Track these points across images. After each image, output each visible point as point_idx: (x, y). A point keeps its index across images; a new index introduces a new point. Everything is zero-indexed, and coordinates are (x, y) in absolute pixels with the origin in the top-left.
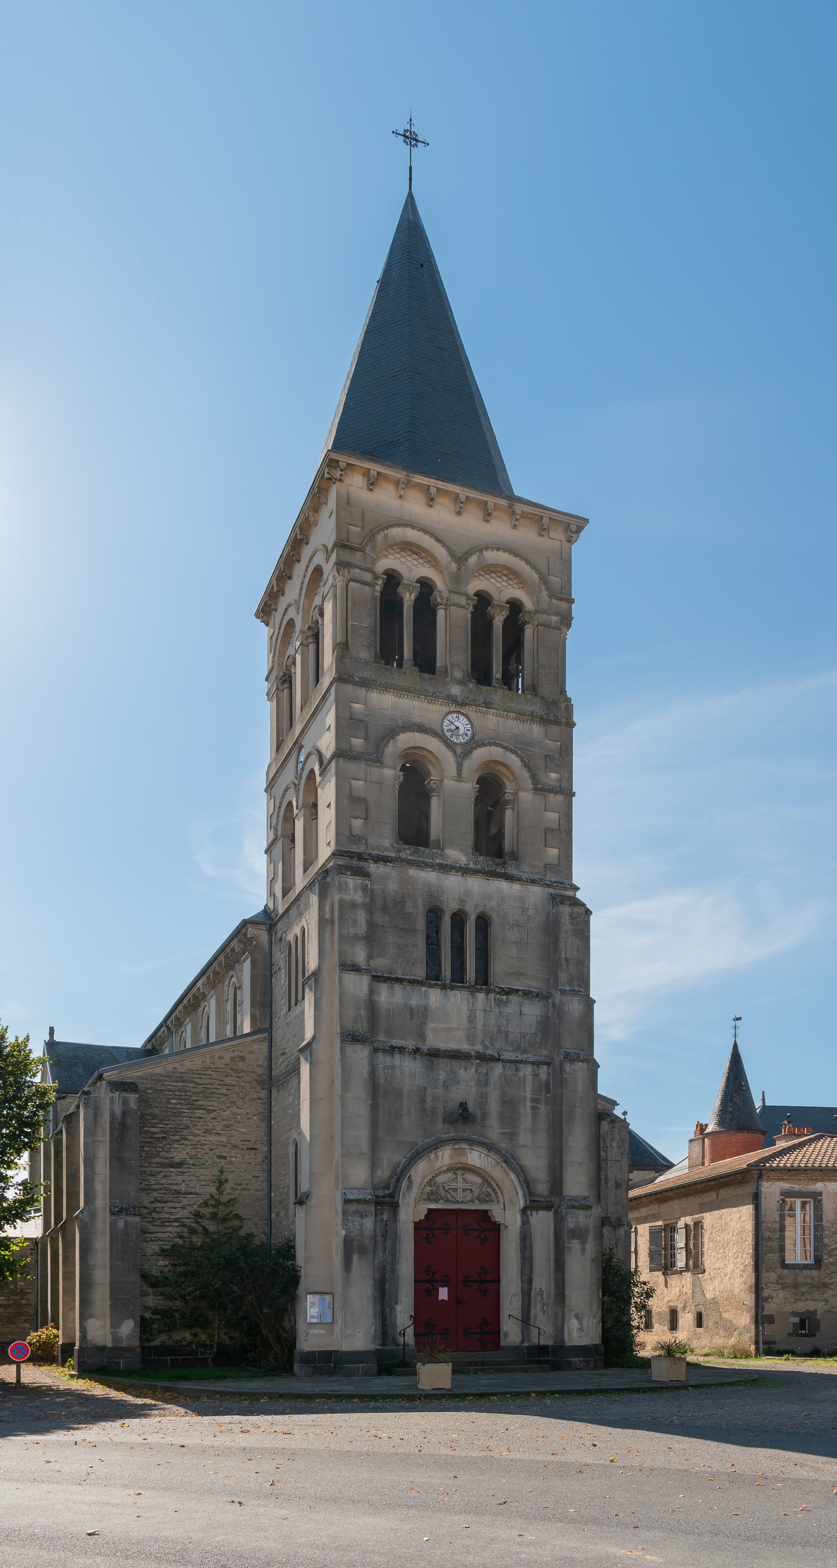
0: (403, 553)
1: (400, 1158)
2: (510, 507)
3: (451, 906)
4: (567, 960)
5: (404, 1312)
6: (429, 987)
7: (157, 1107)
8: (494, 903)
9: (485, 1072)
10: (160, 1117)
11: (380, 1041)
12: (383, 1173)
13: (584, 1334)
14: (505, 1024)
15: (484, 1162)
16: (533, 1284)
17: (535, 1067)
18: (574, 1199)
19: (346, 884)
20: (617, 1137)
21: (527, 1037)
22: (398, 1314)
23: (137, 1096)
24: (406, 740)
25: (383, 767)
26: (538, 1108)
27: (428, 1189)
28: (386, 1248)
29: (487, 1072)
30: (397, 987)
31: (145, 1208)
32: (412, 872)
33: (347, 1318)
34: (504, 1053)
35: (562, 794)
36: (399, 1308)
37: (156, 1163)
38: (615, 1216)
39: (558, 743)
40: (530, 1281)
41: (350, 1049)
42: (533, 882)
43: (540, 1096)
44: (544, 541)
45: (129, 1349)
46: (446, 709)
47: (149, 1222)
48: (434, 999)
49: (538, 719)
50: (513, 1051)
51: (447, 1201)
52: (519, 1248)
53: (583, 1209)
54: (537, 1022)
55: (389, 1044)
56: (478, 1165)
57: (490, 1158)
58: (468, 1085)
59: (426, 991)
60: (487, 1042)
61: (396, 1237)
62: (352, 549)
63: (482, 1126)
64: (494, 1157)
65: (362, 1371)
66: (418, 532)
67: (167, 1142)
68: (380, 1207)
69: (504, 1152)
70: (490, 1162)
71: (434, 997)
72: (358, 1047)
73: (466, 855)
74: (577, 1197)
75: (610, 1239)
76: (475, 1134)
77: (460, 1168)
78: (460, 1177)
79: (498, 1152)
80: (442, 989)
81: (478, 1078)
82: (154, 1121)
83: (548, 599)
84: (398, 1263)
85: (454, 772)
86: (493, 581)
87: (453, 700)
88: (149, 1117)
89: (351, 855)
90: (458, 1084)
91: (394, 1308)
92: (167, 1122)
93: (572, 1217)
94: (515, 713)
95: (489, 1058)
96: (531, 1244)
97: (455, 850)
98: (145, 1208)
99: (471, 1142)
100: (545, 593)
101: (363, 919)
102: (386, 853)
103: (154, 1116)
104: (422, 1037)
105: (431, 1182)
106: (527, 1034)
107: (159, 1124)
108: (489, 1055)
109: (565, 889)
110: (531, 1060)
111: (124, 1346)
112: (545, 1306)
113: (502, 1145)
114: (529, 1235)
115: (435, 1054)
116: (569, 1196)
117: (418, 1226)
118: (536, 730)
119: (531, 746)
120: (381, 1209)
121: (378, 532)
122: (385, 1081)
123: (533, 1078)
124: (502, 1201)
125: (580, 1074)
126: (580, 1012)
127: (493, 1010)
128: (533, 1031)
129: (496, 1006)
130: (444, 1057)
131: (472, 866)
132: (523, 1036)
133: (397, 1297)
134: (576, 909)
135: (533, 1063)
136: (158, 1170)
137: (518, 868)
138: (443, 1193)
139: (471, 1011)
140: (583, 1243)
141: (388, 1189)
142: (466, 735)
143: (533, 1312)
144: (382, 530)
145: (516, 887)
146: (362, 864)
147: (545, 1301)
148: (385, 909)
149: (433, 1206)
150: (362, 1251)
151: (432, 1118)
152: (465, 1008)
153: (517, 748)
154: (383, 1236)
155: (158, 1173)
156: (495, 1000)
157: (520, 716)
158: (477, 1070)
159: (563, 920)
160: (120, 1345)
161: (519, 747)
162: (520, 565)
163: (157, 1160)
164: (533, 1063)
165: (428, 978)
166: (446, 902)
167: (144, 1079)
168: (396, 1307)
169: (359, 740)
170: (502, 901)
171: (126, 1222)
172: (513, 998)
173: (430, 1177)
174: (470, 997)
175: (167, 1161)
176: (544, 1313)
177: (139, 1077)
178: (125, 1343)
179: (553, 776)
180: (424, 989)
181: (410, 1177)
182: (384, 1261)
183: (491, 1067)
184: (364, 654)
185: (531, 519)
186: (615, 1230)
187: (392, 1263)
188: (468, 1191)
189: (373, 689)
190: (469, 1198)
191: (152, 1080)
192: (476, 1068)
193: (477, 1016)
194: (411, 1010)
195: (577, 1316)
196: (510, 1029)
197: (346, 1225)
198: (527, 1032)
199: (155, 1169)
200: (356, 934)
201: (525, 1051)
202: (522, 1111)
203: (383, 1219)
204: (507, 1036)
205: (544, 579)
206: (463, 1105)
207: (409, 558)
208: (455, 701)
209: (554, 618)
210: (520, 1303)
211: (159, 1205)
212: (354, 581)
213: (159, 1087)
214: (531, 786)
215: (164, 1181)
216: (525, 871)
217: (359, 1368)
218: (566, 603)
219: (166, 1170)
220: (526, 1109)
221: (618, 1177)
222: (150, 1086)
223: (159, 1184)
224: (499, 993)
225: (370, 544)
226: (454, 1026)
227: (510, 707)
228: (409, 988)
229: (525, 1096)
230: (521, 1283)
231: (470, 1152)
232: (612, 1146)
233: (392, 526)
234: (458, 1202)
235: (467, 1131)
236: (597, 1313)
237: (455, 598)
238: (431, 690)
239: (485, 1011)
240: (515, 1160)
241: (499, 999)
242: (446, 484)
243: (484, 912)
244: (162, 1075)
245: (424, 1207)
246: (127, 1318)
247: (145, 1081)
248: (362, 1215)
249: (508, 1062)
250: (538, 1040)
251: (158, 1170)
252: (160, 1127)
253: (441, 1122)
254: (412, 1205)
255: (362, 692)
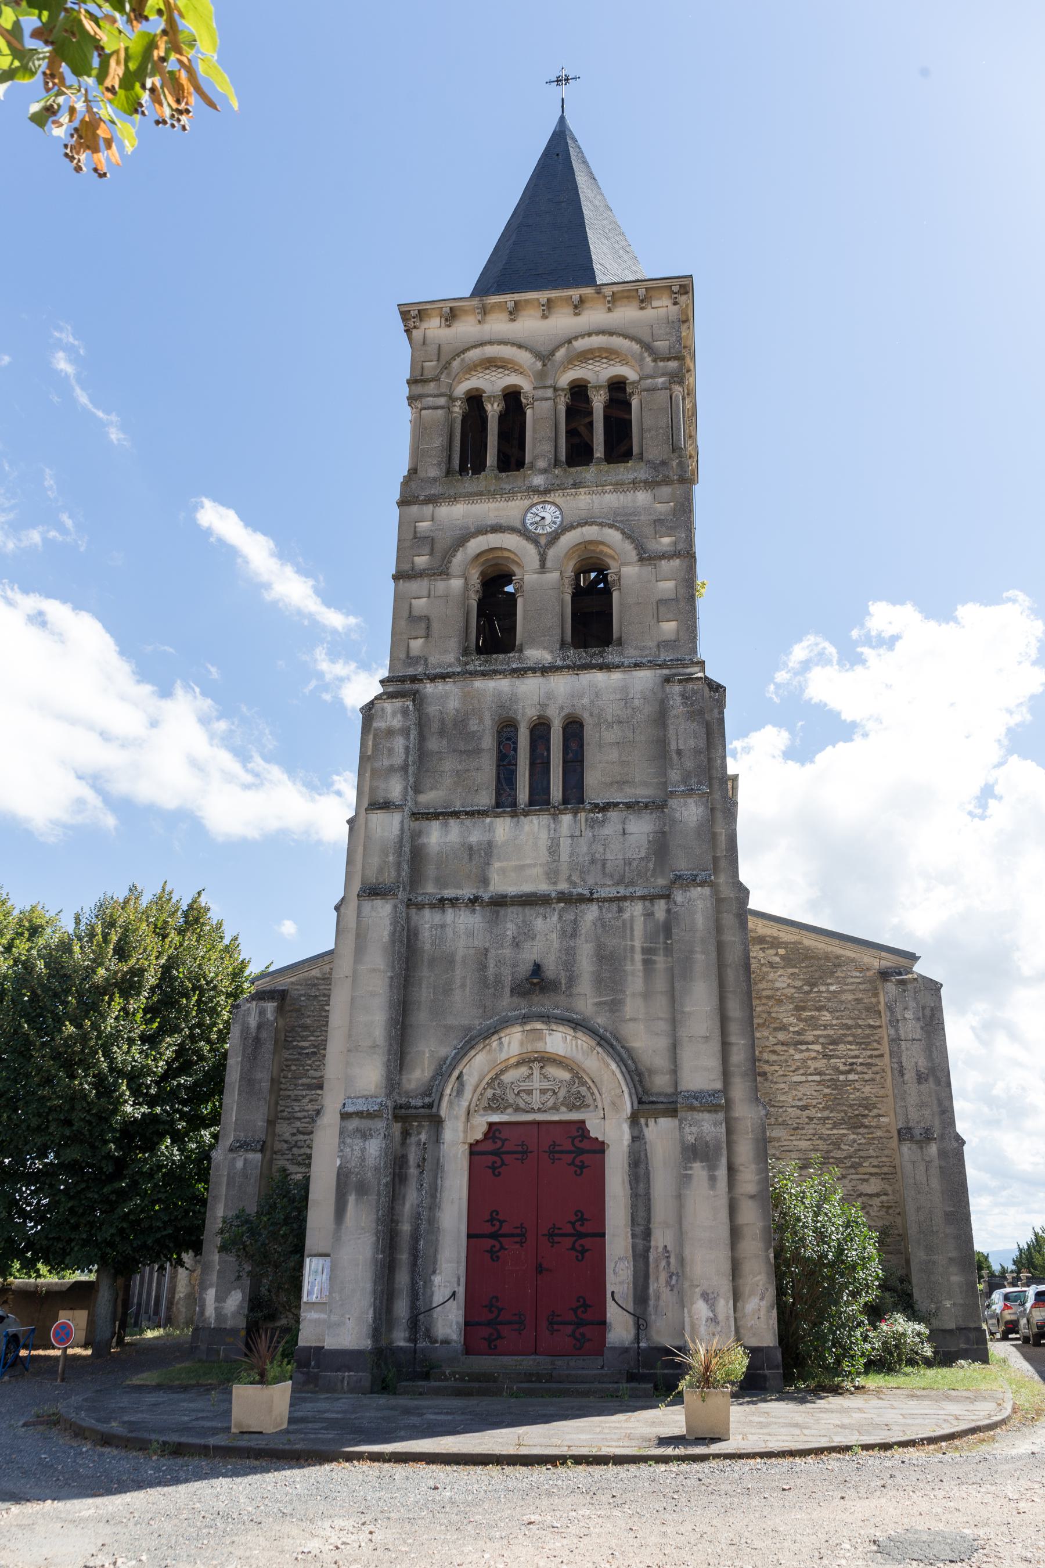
0: (487, 371)
1: (445, 1051)
2: (598, 293)
3: (526, 714)
4: (679, 752)
5: (445, 1287)
6: (495, 817)
7: (309, 1016)
8: (586, 701)
9: (573, 918)
10: (312, 1029)
11: (427, 894)
12: (418, 1075)
13: (719, 1329)
14: (601, 850)
15: (572, 1048)
16: (652, 1238)
17: (647, 903)
18: (696, 1095)
19: (383, 710)
20: (912, 1004)
21: (634, 864)
22: (435, 1289)
23: (275, 1004)
24: (477, 545)
25: (449, 579)
26: (654, 962)
27: (490, 1093)
28: (422, 1185)
29: (576, 918)
30: (452, 822)
31: (286, 1142)
32: (479, 684)
33: (334, 1295)
34: (599, 890)
35: (677, 558)
36: (437, 1279)
37: (303, 1085)
38: (922, 1125)
39: (672, 504)
40: (647, 1234)
41: (367, 905)
42: (637, 665)
43: (656, 943)
44: (649, 313)
45: (233, 1332)
46: (527, 503)
47: (288, 1160)
48: (502, 831)
49: (642, 485)
50: (613, 885)
51: (518, 1109)
52: (627, 1179)
53: (709, 1111)
54: (649, 842)
55: (439, 896)
56: (561, 1052)
57: (579, 1042)
58: (547, 940)
59: (491, 823)
60: (575, 878)
61: (438, 1167)
62: (425, 381)
63: (567, 996)
64: (584, 1039)
65: (348, 1384)
66: (499, 347)
67: (316, 1058)
68: (416, 1124)
69: (601, 1031)
70: (579, 1047)
71: (502, 828)
72: (379, 903)
73: (552, 652)
74: (701, 1092)
75: (914, 1162)
76: (557, 1007)
77: (536, 1060)
78: (536, 1073)
79: (592, 1032)
80: (512, 817)
81: (562, 928)
82: (305, 1033)
83: (653, 364)
84: (439, 1208)
85: (536, 564)
86: (590, 367)
87: (533, 491)
88: (300, 1030)
89: (402, 679)
90: (533, 939)
91: (430, 1280)
92: (319, 1034)
93: (691, 1126)
94: (611, 484)
95: (576, 899)
96: (647, 1174)
97: (538, 650)
98: (286, 1142)
99: (547, 1018)
100: (648, 359)
101: (401, 747)
102: (450, 670)
103: (305, 1027)
104: (485, 881)
105: (495, 1080)
106: (634, 859)
107: (309, 1036)
108: (577, 895)
109: (684, 666)
110: (638, 894)
111: (228, 1327)
112: (674, 1277)
113: (599, 1021)
114: (643, 1157)
115: (500, 902)
116: (688, 1091)
117: (474, 1150)
118: (642, 497)
119: (636, 515)
120: (418, 1126)
121: (453, 358)
122: (432, 945)
123: (645, 919)
124: (600, 1106)
125: (700, 905)
126: (699, 818)
127: (583, 834)
128: (643, 854)
129: (588, 829)
130: (513, 905)
131: (559, 663)
132: (628, 862)
133: (435, 1262)
134: (690, 686)
135: (643, 898)
136: (304, 1093)
137: (621, 654)
138: (511, 1098)
139: (553, 839)
140: (712, 1167)
141: (429, 1095)
142: (554, 523)
143: (652, 1288)
144: (458, 355)
145: (616, 676)
146: (416, 686)
147: (673, 1269)
148: (442, 733)
149: (496, 1118)
150: (362, 1189)
151: (496, 990)
152: (544, 836)
153: (616, 521)
154: (419, 1166)
155: (304, 1097)
156: (587, 820)
157: (619, 486)
158: (560, 917)
159: (671, 703)
160: (223, 1326)
161: (620, 521)
162: (617, 342)
163: (304, 1081)
164: (643, 898)
165: (498, 805)
166: (521, 711)
167: (298, 985)
168: (432, 1278)
169: (424, 558)
170: (597, 696)
171: (245, 1160)
172: (613, 815)
173: (492, 1074)
174: (552, 821)
175: (315, 1081)
176: (672, 1290)
177: (292, 983)
178: (229, 1322)
179: (666, 540)
180: (488, 820)
181: (460, 1076)
182: (418, 1206)
183: (581, 911)
184: (433, 472)
185: (628, 297)
186: (921, 1148)
187: (430, 1208)
188: (550, 1093)
189: (441, 503)
190: (550, 1104)
191: (307, 985)
192: (559, 914)
193: (562, 845)
194: (470, 848)
195: (705, 1296)
196: (609, 856)
197: (342, 1151)
198: (635, 856)
199: (300, 1093)
200: (392, 765)
201: (632, 883)
202: (629, 968)
203: (420, 1140)
204: (604, 866)
205: (647, 347)
206: (537, 969)
207: (494, 374)
208: (536, 491)
209: (661, 380)
210: (630, 1272)
211: (301, 1137)
212: (425, 409)
213: (313, 992)
214: (636, 558)
215: (310, 1107)
216: (631, 654)
217: (343, 1378)
218: (676, 362)
219: (313, 1092)
220: (635, 966)
221: (920, 1064)
222: (303, 992)
223: (304, 1111)
224: (592, 811)
225: (445, 372)
226: (528, 861)
227: (605, 481)
228: (468, 822)
229: (633, 947)
230: (632, 1238)
231: (550, 1034)
232: (905, 1019)
233: (468, 349)
234: (532, 1111)
235: (544, 1004)
236: (767, 1289)
237: (540, 393)
238: (508, 487)
239: (572, 837)
240: (618, 1040)
241: (592, 818)
242: (523, 294)
243: (573, 713)
244: (317, 978)
245: (481, 1123)
246: (235, 1289)
247: (298, 987)
248: (365, 1135)
249: (607, 901)
250: (651, 866)
251: (304, 1093)
252: (311, 1041)
253: (508, 994)
254: (463, 1118)
255: (428, 509)
